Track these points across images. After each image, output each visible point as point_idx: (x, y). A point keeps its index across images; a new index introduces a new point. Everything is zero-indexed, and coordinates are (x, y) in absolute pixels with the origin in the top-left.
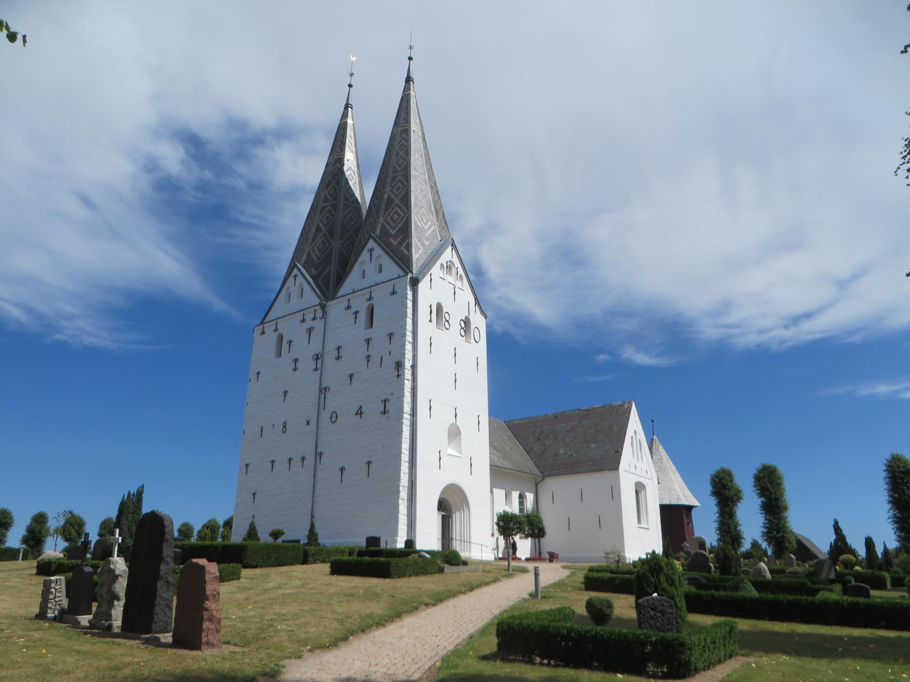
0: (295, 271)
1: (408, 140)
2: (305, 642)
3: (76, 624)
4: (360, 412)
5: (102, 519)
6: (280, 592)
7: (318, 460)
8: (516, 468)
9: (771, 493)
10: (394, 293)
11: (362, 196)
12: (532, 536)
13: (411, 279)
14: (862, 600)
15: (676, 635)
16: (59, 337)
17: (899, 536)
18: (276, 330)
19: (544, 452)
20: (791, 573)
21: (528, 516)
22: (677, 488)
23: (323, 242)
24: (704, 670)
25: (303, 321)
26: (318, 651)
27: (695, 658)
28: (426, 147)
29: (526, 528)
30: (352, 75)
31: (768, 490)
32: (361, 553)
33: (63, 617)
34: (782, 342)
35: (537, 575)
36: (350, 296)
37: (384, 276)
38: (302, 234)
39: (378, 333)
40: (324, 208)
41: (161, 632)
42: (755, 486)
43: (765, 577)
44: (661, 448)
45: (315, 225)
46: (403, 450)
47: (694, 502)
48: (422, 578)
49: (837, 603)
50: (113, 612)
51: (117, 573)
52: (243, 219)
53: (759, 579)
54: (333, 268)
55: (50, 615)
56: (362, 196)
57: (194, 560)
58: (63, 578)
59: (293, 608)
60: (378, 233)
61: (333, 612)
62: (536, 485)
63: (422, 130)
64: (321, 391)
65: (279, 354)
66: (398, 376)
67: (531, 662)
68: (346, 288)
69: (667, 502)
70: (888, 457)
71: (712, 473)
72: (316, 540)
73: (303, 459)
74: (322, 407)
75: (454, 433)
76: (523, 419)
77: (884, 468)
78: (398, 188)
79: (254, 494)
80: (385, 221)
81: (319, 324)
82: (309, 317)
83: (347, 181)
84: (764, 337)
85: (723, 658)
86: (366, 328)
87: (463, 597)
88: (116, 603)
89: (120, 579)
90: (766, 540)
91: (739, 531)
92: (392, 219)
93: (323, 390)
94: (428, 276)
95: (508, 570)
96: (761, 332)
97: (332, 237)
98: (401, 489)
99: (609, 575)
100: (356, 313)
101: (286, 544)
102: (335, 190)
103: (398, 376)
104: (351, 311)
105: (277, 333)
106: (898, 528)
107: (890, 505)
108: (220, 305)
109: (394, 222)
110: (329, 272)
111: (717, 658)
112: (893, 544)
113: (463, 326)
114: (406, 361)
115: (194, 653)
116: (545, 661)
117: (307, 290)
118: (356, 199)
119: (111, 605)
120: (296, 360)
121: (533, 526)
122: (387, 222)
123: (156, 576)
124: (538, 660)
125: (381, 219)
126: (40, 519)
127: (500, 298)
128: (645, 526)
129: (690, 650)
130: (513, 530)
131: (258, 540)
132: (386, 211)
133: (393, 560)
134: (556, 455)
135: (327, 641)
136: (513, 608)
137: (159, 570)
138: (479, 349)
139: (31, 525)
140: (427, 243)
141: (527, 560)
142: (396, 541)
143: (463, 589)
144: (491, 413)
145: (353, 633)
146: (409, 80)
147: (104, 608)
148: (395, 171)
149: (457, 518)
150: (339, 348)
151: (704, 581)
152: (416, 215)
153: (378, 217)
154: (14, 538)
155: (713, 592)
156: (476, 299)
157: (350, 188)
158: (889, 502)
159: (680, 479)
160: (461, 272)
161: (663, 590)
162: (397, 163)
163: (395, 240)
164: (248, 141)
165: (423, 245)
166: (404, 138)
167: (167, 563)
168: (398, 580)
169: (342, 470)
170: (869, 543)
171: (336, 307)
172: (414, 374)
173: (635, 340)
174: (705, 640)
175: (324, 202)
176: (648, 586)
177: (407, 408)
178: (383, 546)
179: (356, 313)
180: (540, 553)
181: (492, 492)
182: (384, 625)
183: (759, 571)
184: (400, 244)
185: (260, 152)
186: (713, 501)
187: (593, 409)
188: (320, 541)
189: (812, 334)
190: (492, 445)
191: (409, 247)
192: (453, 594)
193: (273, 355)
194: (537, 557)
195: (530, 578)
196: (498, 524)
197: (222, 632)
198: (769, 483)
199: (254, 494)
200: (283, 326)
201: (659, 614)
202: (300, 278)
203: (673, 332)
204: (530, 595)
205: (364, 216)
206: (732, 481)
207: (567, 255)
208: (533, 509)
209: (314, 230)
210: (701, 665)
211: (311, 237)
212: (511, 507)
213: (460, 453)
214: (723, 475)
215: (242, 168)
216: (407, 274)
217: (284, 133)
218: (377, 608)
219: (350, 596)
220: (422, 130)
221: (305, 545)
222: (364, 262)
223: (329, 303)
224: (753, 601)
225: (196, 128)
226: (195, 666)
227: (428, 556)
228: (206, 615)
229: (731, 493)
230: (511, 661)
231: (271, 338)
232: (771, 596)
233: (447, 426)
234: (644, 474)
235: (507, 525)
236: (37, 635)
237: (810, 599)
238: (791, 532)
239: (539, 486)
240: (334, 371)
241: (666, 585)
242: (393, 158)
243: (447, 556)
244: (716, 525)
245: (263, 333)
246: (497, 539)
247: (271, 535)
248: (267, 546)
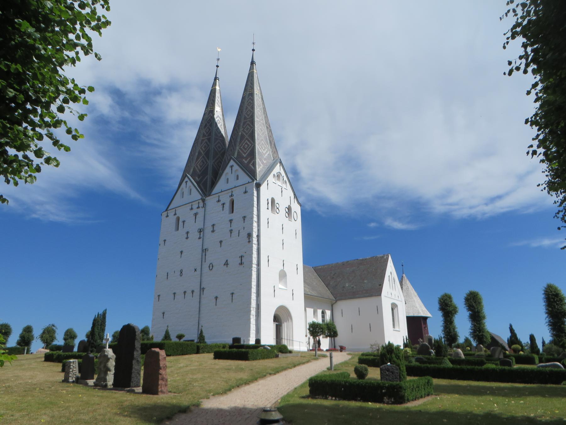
0: (186, 179)
1: (253, 100)
2: (210, 391)
3: (86, 384)
4: (226, 264)
5: (66, 329)
6: (188, 368)
8: (320, 296)
9: (475, 309)
10: (246, 192)
12: (330, 336)
14: (507, 368)
15: (398, 382)
16: (34, 216)
17: (552, 334)
18: (175, 214)
19: (336, 285)
20: (478, 355)
21: (327, 324)
22: (418, 306)
23: (202, 161)
24: (413, 400)
25: (192, 209)
26: (217, 396)
28: (263, 103)
30: (218, 59)
31: (473, 307)
32: (231, 347)
33: (77, 381)
34: (484, 214)
35: (331, 357)
36: (220, 194)
37: (240, 182)
39: (236, 216)
40: (203, 140)
41: (135, 387)
42: (465, 304)
43: (460, 357)
44: (408, 282)
45: (197, 151)
46: (253, 286)
47: (428, 314)
48: (266, 361)
49: (493, 370)
50: (107, 377)
51: (109, 357)
52: (148, 141)
53: (457, 358)
54: (209, 176)
55: (71, 380)
57: (153, 349)
58: (76, 360)
60: (236, 156)
62: (332, 306)
63: (261, 93)
64: (203, 251)
65: (177, 229)
66: (249, 242)
67: (326, 398)
68: (217, 189)
69: (411, 315)
70: (545, 286)
71: (439, 297)
72: (204, 339)
73: (193, 292)
74: (204, 260)
75: (283, 275)
76: (324, 266)
77: (543, 292)
79: (163, 313)
80: (240, 148)
81: (201, 211)
82: (195, 206)
84: (473, 211)
85: (423, 395)
86: (230, 213)
87: (290, 370)
88: (109, 373)
89: (111, 360)
90: (473, 337)
91: (456, 332)
92: (244, 147)
94: (266, 182)
95: (316, 356)
96: (471, 208)
97: (208, 158)
98: (252, 309)
99: (372, 357)
100: (223, 204)
102: (210, 129)
103: (249, 242)
105: (176, 216)
106: (551, 329)
108: (134, 195)
109: (245, 149)
110: (207, 179)
111: (420, 395)
112: (548, 338)
113: (287, 210)
115: (156, 396)
116: (334, 398)
117: (194, 190)
118: (222, 135)
119: (106, 374)
120: (188, 233)
121: (329, 330)
122: (241, 149)
123: (132, 357)
125: (238, 148)
126: (28, 330)
127: (309, 188)
128: (398, 329)
129: (405, 390)
130: (318, 333)
131: (171, 340)
132: (240, 142)
133: (250, 351)
134: (344, 287)
135: (221, 391)
136: (317, 376)
137: (133, 355)
138: (297, 225)
139: (22, 333)
140: (265, 162)
141: (327, 350)
142: (249, 340)
145: (233, 387)
146: (253, 63)
147: (102, 375)
148: (245, 118)
149: (285, 326)
150: (213, 225)
151: (425, 360)
153: (235, 145)
154: (12, 341)
156: (295, 194)
157: (218, 128)
158: (546, 313)
159: (419, 301)
160: (285, 178)
161: (394, 362)
162: (246, 114)
163: (246, 160)
164: (151, 93)
165: (263, 163)
167: (137, 351)
168: (253, 362)
169: (216, 298)
170: (532, 338)
171: (211, 201)
173: (393, 213)
174: (413, 385)
175: (203, 137)
176: (386, 359)
177: (255, 261)
178: (242, 343)
179: (223, 204)
181: (305, 310)
182: (249, 384)
183: (457, 354)
184: (249, 162)
185: (159, 99)
186: (440, 314)
187: (366, 259)
188: (206, 340)
189: (502, 208)
190: (305, 281)
191: (254, 165)
192: (284, 369)
193: (174, 229)
194: (333, 348)
196: (309, 329)
197: (169, 386)
198: (473, 303)
199: (163, 313)
200: (180, 212)
202: (189, 183)
203: (416, 208)
204: (328, 369)
205: (227, 145)
206: (451, 301)
207: (350, 161)
208: (330, 320)
209: (197, 154)
210: (411, 398)
212: (317, 319)
213: (286, 287)
214: (445, 298)
215: (147, 110)
216: (253, 181)
217: (173, 88)
218: (244, 376)
219: (228, 370)
220: (261, 93)
221: (197, 343)
223: (207, 198)
225: (119, 85)
226: (159, 401)
227: (269, 348)
228: (160, 377)
229: (451, 309)
230: (316, 398)
231: (172, 219)
232: (459, 367)
233: (278, 272)
234: (397, 298)
235: (315, 330)
237: (479, 368)
239: (334, 306)
240: (210, 239)
242: (244, 110)
243: (280, 348)
244: (442, 328)
245: (167, 216)
246: (309, 338)
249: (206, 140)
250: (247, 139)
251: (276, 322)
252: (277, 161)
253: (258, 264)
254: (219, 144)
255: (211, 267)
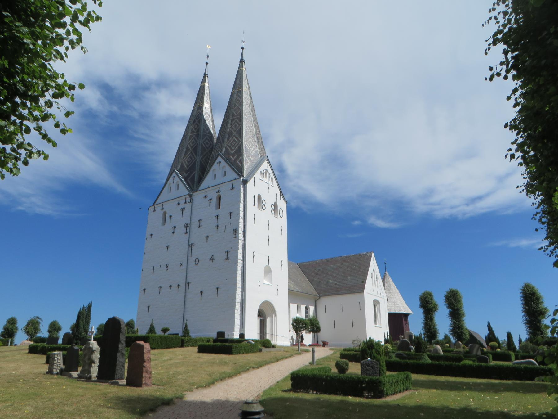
0: (174, 174)
1: (241, 97)
2: (193, 384)
3: (71, 376)
4: (212, 259)
5: (50, 322)
6: (172, 362)
7: (187, 286)
10: (233, 188)
11: (214, 129)
12: (313, 331)
13: (243, 180)
14: (483, 364)
15: (378, 377)
16: (20, 208)
17: (529, 332)
18: (162, 209)
19: (320, 282)
20: (456, 352)
21: (311, 320)
22: (399, 303)
23: (190, 157)
24: (392, 395)
25: (179, 204)
27: (386, 388)
28: (252, 101)
29: (309, 327)
30: (208, 57)
31: (453, 304)
32: (215, 341)
33: (62, 373)
35: (313, 352)
36: (207, 190)
38: (178, 152)
39: (223, 212)
40: (191, 136)
42: (445, 302)
43: (439, 353)
44: (390, 279)
45: (185, 147)
48: (250, 355)
49: (471, 366)
51: (94, 349)
52: (136, 136)
54: (197, 173)
55: (55, 372)
56: (214, 129)
57: (138, 342)
58: (61, 352)
59: (183, 369)
60: (223, 152)
61: (205, 371)
63: (250, 91)
64: (189, 246)
65: (164, 223)
66: (235, 237)
67: (308, 392)
68: (204, 185)
69: (393, 311)
70: (523, 285)
71: (421, 294)
72: (188, 333)
73: (178, 286)
74: (190, 255)
75: (268, 271)
78: (235, 126)
79: (149, 307)
81: (188, 206)
82: (182, 202)
83: (204, 120)
84: (454, 211)
85: (402, 390)
86: (216, 209)
88: (93, 365)
89: (95, 353)
90: (452, 334)
91: (436, 329)
93: (191, 245)
95: (298, 350)
96: (452, 208)
98: (236, 303)
99: (354, 352)
100: (210, 200)
101: (172, 336)
103: (235, 237)
104: (209, 198)
106: (528, 327)
107: (524, 313)
108: (120, 189)
109: (233, 146)
110: (194, 175)
114: (240, 229)
117: (181, 185)
118: (210, 131)
119: (90, 366)
120: (174, 227)
122: (229, 146)
124: (311, 391)
125: (225, 144)
126: (12, 322)
128: (379, 326)
129: (384, 384)
130: (302, 328)
131: (155, 333)
132: (228, 139)
133: (234, 345)
134: (328, 283)
135: (204, 384)
136: (299, 371)
137: (118, 347)
138: (283, 221)
140: (252, 159)
141: (310, 345)
143: (273, 360)
144: (289, 259)
145: (217, 381)
146: (242, 61)
147: (87, 367)
148: (233, 115)
149: (269, 321)
150: (200, 221)
152: (246, 142)
153: (223, 142)
155: (408, 361)
156: (281, 192)
157: (207, 125)
159: (401, 298)
160: (272, 176)
161: (374, 357)
163: (233, 157)
164: (140, 88)
165: (250, 160)
166: (239, 96)
167: (122, 344)
168: (237, 356)
169: (202, 292)
171: (198, 196)
172: (244, 237)
173: (376, 212)
174: (392, 380)
175: (191, 133)
176: (367, 355)
177: (240, 256)
178: (226, 337)
179: (210, 200)
180: (317, 342)
181: (289, 305)
182: (232, 377)
183: (436, 350)
184: (236, 159)
185: (147, 94)
186: (421, 311)
187: (349, 257)
188: (190, 334)
190: (289, 277)
191: (242, 161)
194: (316, 344)
195: (310, 355)
196: (293, 325)
198: (453, 301)
199: (149, 307)
200: (167, 207)
201: (371, 368)
202: (177, 179)
203: (399, 207)
204: (310, 363)
205: (215, 142)
206: (432, 299)
207: (335, 160)
208: (314, 315)
209: (185, 150)
210: (389, 392)
211: (183, 153)
213: (271, 282)
214: (427, 295)
215: (136, 105)
216: (240, 178)
217: (162, 84)
218: (228, 369)
219: (212, 363)
220: (250, 91)
221: (182, 336)
222: (215, 169)
223: (194, 194)
224: (428, 365)
226: (143, 394)
227: (253, 342)
228: (144, 369)
230: (298, 392)
231: (160, 214)
234: (379, 295)
235: (298, 325)
236: (54, 381)
237: (457, 364)
238: (467, 329)
239: (318, 302)
240: (197, 235)
241: (375, 354)
243: (264, 342)
244: (422, 325)
245: (154, 211)
247: (162, 331)
248: (161, 337)
249: (194, 136)
250: (235, 136)
251: (261, 317)
252: (264, 158)
253: (244, 260)
254: (207, 141)
255: (197, 261)
